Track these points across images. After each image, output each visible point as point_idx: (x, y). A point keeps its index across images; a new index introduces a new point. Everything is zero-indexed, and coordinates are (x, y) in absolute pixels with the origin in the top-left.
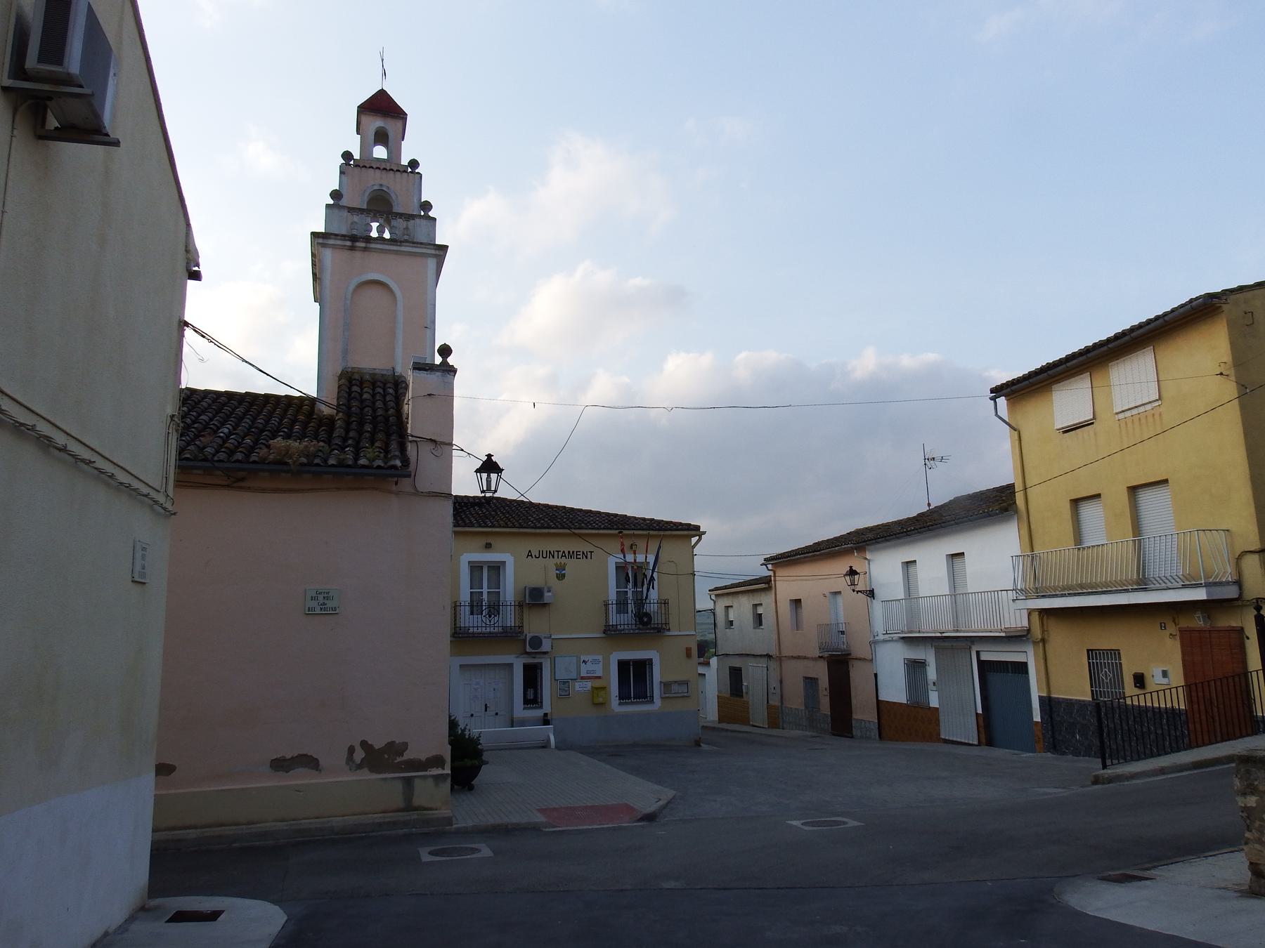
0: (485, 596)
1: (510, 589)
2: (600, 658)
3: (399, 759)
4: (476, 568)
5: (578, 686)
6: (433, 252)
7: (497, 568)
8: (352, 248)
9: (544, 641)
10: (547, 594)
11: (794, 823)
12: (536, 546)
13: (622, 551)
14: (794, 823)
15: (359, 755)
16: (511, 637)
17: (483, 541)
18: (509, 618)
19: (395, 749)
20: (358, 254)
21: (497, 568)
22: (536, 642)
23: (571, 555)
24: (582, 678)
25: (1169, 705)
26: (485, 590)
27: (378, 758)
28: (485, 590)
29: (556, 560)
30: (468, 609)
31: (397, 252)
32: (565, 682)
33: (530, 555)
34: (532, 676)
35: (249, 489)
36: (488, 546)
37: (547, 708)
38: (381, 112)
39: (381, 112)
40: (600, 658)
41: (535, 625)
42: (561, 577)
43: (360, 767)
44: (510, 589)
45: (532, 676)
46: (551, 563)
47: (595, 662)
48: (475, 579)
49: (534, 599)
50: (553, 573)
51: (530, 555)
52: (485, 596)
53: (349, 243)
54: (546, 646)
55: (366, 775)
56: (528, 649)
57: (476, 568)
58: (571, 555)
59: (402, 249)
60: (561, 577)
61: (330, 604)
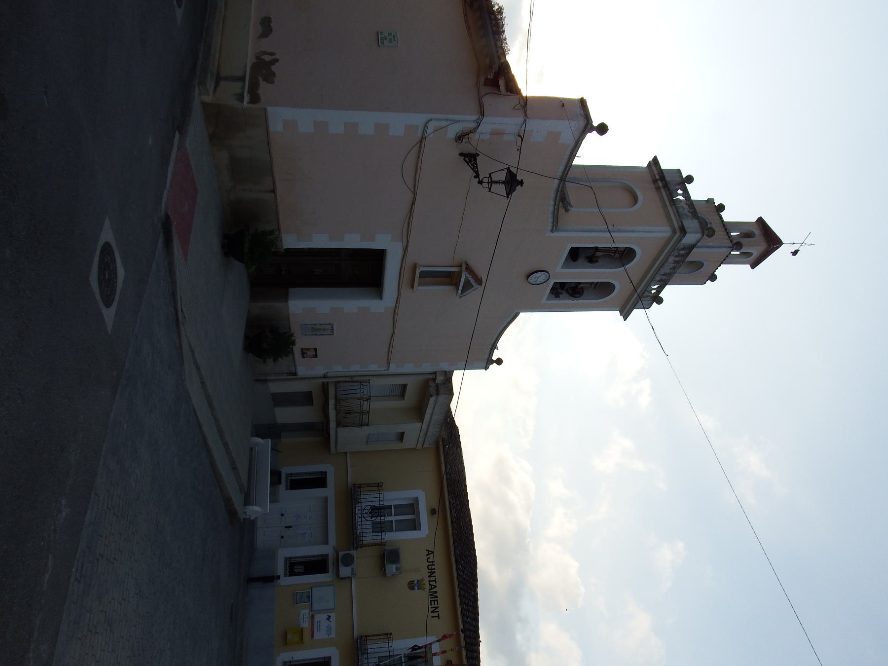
0: (388, 518)
1: (394, 537)
2: (333, 635)
3: (260, 79)
4: (412, 507)
5: (305, 612)
6: (676, 226)
7: (414, 525)
8: (655, 181)
9: (349, 568)
10: (394, 567)
11: (150, 142)
12: (439, 559)
13: (444, 652)
14: (150, 142)
15: (267, 58)
16: (352, 540)
17: (436, 506)
18: (369, 537)
19: (270, 77)
20: (652, 186)
21: (414, 525)
22: (348, 561)
23: (433, 595)
24: (313, 617)
25: (375, 405)
26: (393, 518)
27: (264, 69)
28: (393, 518)
29: (426, 582)
30: (377, 504)
31: (665, 206)
32: (309, 597)
33: (430, 552)
34: (316, 566)
35: (466, 16)
36: (433, 512)
37: (287, 581)
38: (758, 242)
39: (758, 242)
40: (333, 635)
41: (364, 560)
42: (411, 586)
43: (258, 58)
44: (394, 537)
45: (316, 566)
46: (424, 574)
47: (329, 629)
48: (400, 509)
49: (389, 557)
50: (415, 577)
51: (430, 552)
52: (388, 518)
53: (658, 177)
54: (345, 571)
55: (250, 61)
56: (341, 554)
57: (412, 507)
58: (433, 595)
59: (669, 208)
60: (411, 586)
61: (386, 42)
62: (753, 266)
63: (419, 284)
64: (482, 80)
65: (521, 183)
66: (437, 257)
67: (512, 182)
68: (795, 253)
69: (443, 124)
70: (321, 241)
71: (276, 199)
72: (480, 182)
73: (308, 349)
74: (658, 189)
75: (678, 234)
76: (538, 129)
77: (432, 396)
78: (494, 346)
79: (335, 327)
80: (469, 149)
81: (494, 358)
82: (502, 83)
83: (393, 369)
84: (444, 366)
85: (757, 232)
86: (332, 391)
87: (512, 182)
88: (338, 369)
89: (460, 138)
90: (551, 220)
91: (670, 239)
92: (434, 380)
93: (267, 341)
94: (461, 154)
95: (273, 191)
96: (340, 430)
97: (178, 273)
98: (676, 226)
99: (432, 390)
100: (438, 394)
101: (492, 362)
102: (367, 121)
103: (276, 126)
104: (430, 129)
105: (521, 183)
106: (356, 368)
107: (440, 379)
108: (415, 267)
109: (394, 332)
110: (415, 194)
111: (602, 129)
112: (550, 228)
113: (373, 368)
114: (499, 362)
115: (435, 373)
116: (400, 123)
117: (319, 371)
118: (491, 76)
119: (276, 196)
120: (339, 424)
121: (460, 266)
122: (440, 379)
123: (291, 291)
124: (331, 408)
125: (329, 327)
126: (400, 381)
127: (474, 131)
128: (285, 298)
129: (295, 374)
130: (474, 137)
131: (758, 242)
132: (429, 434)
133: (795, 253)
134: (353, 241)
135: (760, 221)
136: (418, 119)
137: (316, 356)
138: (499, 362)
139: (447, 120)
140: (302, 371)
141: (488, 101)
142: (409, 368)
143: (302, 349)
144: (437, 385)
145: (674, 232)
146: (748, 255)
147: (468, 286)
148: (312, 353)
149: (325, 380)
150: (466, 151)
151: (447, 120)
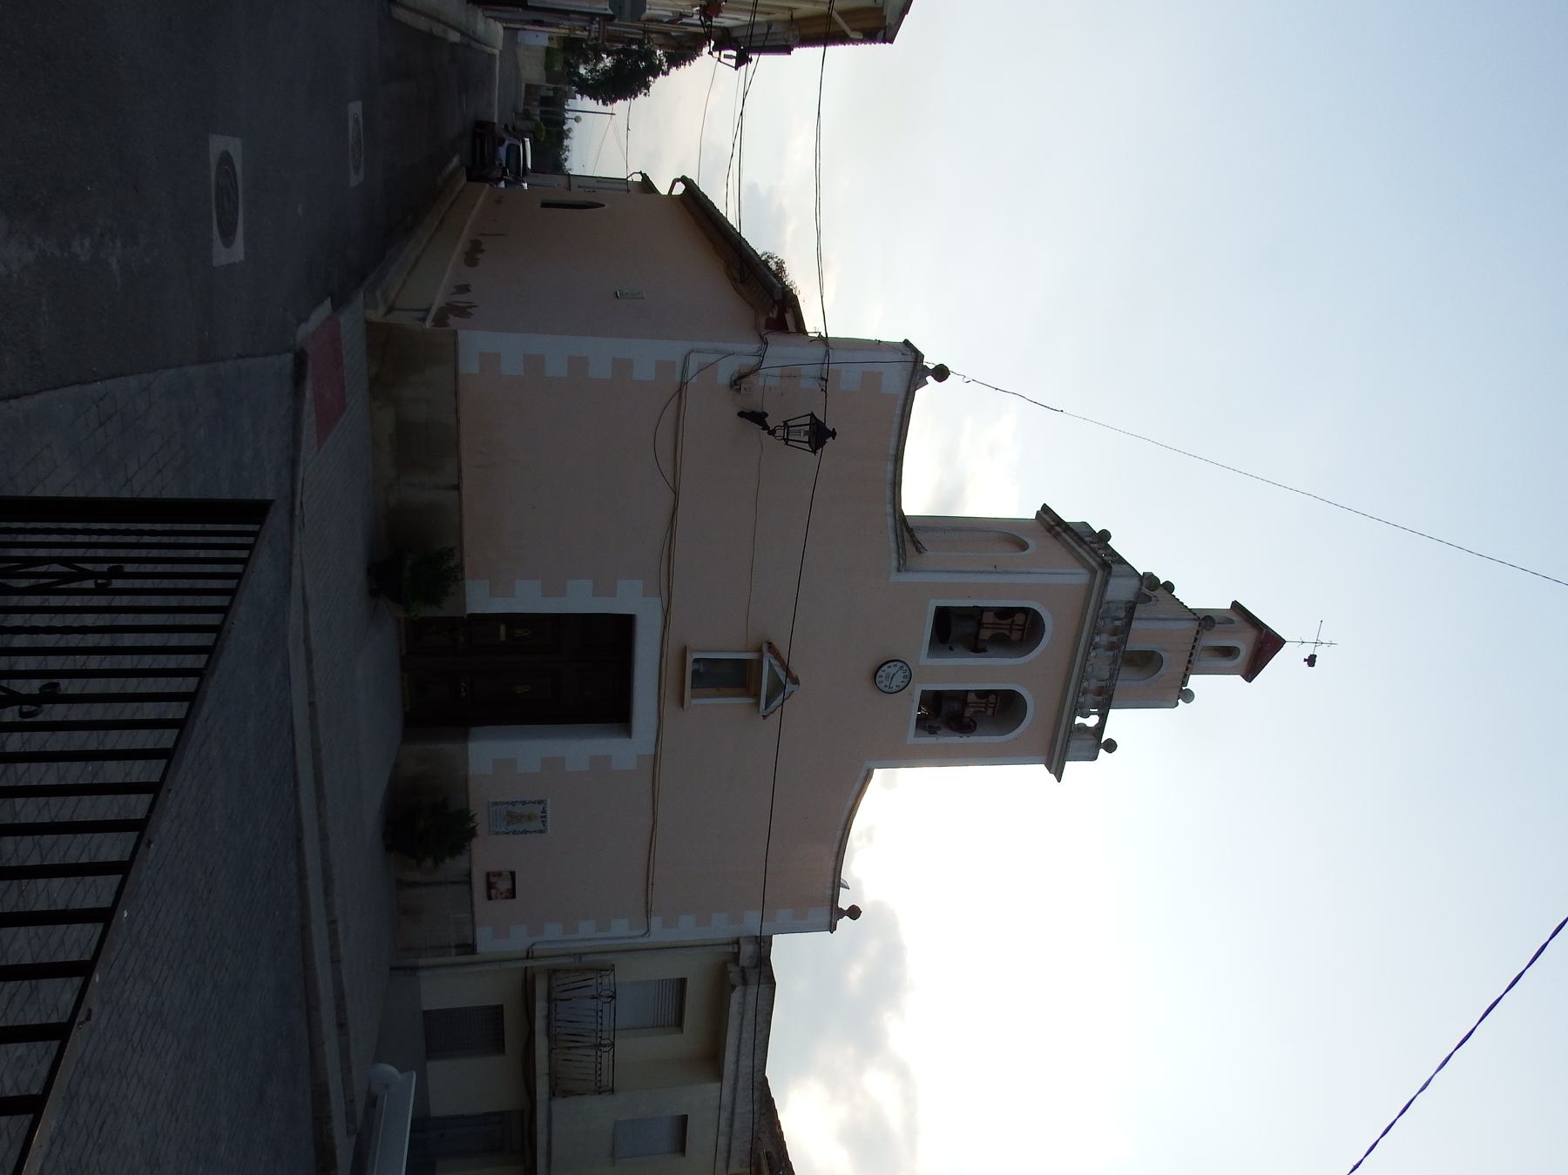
6: (1094, 564)
39: (1246, 643)
62: (1250, 675)
63: (693, 697)
64: (763, 321)
65: (833, 434)
66: (723, 641)
67: (819, 435)
68: (1311, 661)
69: (710, 358)
70: (528, 598)
71: (460, 501)
72: (772, 433)
73: (499, 874)
74: (1057, 536)
75: (1100, 574)
76: (848, 378)
77: (733, 987)
78: (837, 884)
79: (548, 809)
80: (753, 405)
81: (844, 904)
82: (789, 317)
83: (660, 933)
84: (751, 923)
85: (1235, 618)
86: (541, 988)
87: (819, 435)
88: (554, 936)
89: (737, 382)
90: (893, 545)
91: (1090, 587)
92: (736, 957)
93: (426, 826)
94: (741, 414)
95: (457, 487)
96: (559, 1104)
97: (310, 364)
98: (1094, 564)
99: (734, 976)
100: (745, 983)
101: (841, 913)
102: (601, 353)
103: (469, 365)
104: (693, 367)
105: (833, 434)
106: (587, 934)
107: (747, 950)
108: (684, 651)
109: (655, 822)
110: (676, 493)
111: (941, 373)
112: (894, 563)
113: (621, 929)
114: (854, 913)
115: (737, 942)
116: (650, 356)
117: (517, 940)
118: (774, 315)
119: (460, 495)
120: (553, 1094)
121: (760, 650)
122: (747, 950)
123: (474, 730)
124: (537, 1023)
125: (537, 810)
126: (670, 968)
127: (755, 370)
128: (465, 737)
129: (469, 948)
130: (758, 381)
131: (1246, 643)
132: (737, 1125)
133: (1311, 661)
134: (580, 599)
135: (1236, 605)
136: (672, 350)
137: (512, 894)
138: (854, 913)
139: (716, 352)
140: (487, 943)
141: (771, 338)
142: (687, 929)
143: (488, 875)
144: (743, 970)
145: (1093, 572)
146: (1229, 652)
147: (777, 688)
148: (504, 885)
149: (529, 963)
150: (748, 408)
151: (716, 352)
